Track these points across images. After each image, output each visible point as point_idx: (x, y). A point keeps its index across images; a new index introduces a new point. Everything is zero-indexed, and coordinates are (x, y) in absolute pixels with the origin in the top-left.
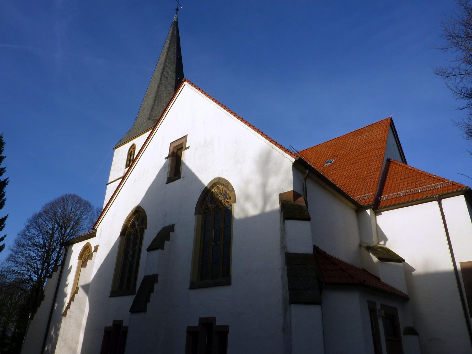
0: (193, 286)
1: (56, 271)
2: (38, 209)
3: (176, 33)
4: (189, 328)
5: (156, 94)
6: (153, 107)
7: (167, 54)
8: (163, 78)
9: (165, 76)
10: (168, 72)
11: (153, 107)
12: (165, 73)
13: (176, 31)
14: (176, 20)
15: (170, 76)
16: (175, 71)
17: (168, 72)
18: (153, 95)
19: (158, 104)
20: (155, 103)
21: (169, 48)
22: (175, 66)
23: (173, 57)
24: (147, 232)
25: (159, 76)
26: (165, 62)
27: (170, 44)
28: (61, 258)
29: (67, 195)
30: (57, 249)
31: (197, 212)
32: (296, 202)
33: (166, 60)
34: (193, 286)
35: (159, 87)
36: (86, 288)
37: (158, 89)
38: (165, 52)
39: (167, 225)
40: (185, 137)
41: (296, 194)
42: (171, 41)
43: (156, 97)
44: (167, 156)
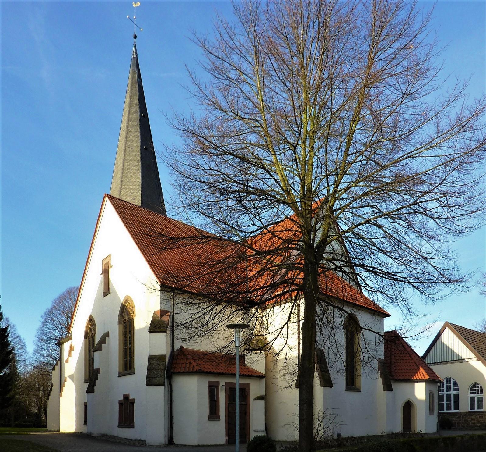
0: (120, 375)
1: (57, 365)
2: (48, 305)
3: (136, 78)
4: (119, 400)
5: (122, 174)
6: (120, 191)
7: (129, 113)
8: (128, 150)
9: (129, 147)
10: (131, 141)
11: (120, 191)
12: (129, 143)
13: (136, 74)
14: (135, 56)
15: (135, 145)
16: (139, 137)
17: (131, 141)
18: (119, 175)
19: (126, 186)
20: (121, 185)
21: (130, 104)
22: (138, 131)
23: (136, 117)
24: (96, 336)
25: (123, 148)
26: (128, 127)
27: (131, 97)
28: (128, 326)
29: (71, 288)
30: (296, 242)
31: (119, 323)
32: (161, 319)
33: (128, 123)
34: (120, 375)
35: (124, 164)
36: (71, 377)
37: (123, 167)
38: (126, 109)
39: (106, 332)
40: (109, 256)
41: (163, 312)
42: (131, 92)
43: (122, 178)
44: (101, 273)
